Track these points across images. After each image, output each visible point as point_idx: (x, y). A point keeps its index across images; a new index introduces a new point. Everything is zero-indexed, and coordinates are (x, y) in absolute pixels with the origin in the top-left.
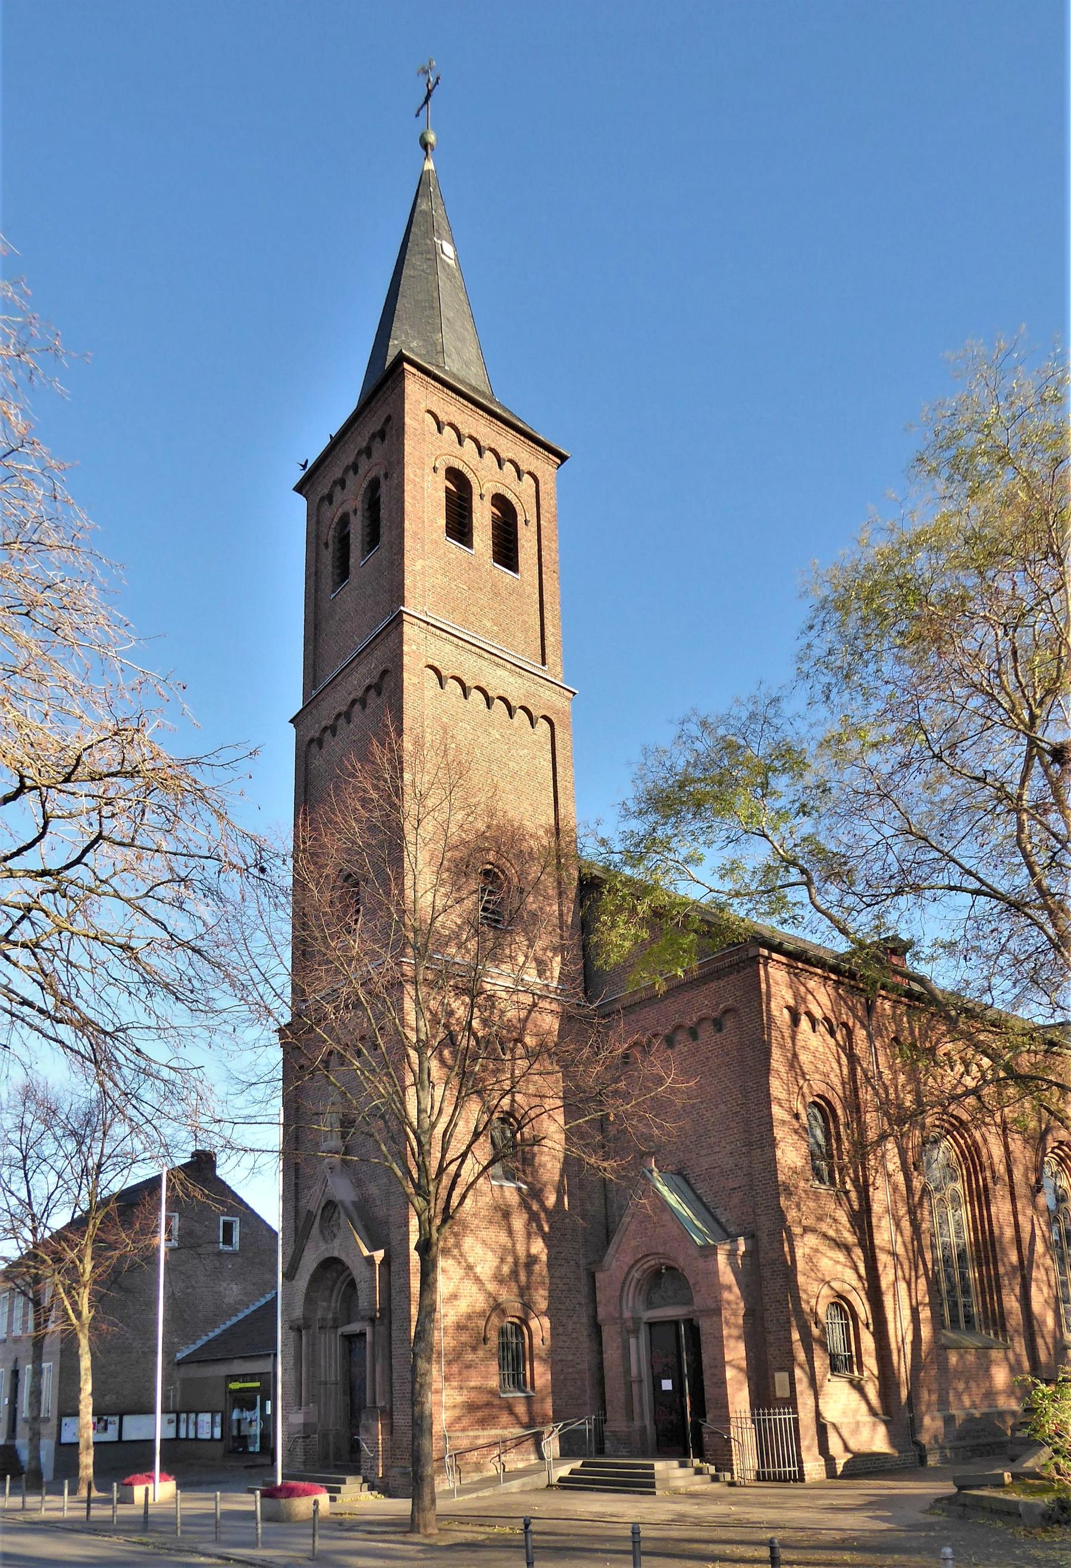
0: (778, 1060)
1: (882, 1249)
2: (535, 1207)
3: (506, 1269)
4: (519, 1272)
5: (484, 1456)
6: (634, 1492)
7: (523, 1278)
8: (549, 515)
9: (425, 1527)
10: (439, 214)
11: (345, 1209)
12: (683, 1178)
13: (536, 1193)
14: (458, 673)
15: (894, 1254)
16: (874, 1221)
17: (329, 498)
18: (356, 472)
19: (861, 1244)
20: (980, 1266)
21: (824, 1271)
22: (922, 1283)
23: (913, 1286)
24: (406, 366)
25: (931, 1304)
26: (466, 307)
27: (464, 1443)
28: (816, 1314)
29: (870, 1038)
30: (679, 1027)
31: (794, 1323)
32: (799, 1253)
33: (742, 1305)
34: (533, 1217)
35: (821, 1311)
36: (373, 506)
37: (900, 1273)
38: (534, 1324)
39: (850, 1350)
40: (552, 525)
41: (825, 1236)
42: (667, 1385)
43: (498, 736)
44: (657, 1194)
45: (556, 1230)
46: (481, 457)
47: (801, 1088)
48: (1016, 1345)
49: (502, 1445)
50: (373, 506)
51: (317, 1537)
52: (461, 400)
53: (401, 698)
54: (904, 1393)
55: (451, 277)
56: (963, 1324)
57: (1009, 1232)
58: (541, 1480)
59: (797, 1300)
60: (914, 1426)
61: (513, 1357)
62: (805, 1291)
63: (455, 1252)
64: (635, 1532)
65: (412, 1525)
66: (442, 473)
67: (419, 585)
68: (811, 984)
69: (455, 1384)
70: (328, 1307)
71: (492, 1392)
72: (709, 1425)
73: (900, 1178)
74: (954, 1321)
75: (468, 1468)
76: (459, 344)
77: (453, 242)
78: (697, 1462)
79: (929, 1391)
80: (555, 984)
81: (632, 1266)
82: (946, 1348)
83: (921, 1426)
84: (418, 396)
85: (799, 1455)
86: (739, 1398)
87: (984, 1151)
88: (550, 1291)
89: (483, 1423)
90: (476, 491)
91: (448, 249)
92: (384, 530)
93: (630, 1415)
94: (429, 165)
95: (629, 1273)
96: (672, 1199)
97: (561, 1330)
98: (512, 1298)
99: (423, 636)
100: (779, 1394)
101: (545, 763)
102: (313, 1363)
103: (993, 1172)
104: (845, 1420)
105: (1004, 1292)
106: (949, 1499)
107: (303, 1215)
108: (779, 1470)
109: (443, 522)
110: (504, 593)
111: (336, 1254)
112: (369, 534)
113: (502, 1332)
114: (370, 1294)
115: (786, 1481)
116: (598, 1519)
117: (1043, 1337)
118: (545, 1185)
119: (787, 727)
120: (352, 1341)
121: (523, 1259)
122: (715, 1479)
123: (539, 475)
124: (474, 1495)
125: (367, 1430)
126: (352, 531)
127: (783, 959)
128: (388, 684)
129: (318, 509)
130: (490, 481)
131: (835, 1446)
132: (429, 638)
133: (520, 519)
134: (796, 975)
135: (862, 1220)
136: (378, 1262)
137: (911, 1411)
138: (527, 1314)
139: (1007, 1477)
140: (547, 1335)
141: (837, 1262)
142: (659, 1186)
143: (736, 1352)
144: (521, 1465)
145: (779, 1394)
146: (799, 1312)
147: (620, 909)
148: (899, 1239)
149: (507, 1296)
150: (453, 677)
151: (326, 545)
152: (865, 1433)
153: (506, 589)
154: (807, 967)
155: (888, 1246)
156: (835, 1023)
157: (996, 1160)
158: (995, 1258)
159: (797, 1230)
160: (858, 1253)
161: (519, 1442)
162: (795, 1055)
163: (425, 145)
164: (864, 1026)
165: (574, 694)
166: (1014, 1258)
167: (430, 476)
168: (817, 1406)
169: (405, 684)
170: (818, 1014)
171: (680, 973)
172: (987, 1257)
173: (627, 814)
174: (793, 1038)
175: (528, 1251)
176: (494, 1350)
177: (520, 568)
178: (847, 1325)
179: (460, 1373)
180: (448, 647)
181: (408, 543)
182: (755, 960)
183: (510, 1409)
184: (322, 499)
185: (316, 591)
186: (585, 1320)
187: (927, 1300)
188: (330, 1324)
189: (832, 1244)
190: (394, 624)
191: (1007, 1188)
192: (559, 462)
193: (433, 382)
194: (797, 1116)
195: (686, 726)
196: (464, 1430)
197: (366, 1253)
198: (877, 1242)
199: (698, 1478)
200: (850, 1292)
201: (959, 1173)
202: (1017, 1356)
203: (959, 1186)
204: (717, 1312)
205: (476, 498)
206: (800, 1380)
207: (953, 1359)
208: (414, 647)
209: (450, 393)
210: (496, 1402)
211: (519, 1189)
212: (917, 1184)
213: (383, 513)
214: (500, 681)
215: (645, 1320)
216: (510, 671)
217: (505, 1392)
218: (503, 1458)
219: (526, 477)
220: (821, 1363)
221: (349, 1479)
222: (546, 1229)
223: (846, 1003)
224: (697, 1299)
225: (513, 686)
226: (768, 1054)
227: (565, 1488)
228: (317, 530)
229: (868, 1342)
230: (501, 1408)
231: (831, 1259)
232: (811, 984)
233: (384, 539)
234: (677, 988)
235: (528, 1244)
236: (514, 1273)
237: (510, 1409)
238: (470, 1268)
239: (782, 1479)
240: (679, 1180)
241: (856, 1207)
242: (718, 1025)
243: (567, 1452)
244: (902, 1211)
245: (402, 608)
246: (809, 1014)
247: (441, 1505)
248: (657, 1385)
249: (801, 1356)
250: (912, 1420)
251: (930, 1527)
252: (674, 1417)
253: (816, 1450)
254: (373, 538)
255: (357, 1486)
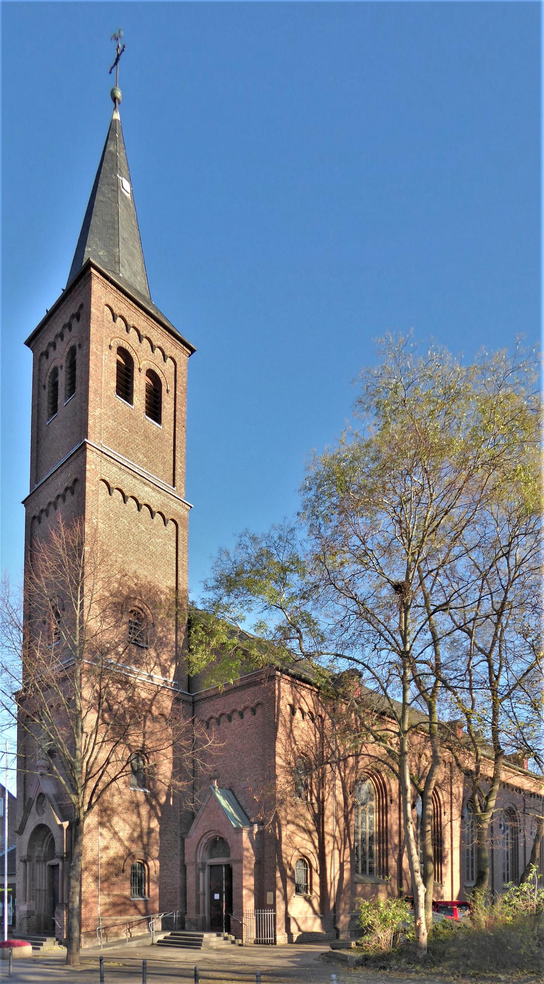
0: (281, 733)
1: (328, 834)
2: (154, 803)
3: (136, 834)
4: (142, 837)
5: (120, 929)
6: (191, 948)
7: (145, 840)
8: (182, 388)
9: (73, 962)
10: (121, 155)
11: (49, 798)
12: (231, 792)
13: (155, 795)
14: (120, 486)
15: (334, 837)
16: (325, 819)
17: (46, 354)
18: (62, 340)
19: (318, 830)
20: (379, 843)
21: (296, 843)
22: (347, 852)
23: (342, 852)
24: (93, 270)
25: (351, 862)
26: (136, 231)
27: (109, 922)
28: (290, 865)
29: (333, 725)
30: (234, 711)
31: (278, 868)
32: (284, 834)
33: (254, 858)
34: (152, 807)
35: (293, 863)
36: (72, 366)
37: (336, 846)
38: (151, 863)
39: (307, 882)
40: (183, 395)
41: (298, 825)
42: (217, 896)
43: (144, 529)
44: (217, 800)
45: (166, 815)
46: (140, 342)
47: (293, 749)
48: (392, 883)
49: (130, 925)
50: (72, 366)
51: (11, 966)
52: (129, 300)
53: (84, 499)
54: (332, 904)
55: (127, 206)
56: (368, 872)
57: (395, 828)
58: (148, 942)
59: (281, 857)
60: (335, 920)
61: (139, 880)
62: (285, 853)
63: (108, 824)
64: (144, 963)
65: (67, 961)
66: (115, 350)
67: (97, 425)
68: (304, 693)
69: (105, 893)
70: (40, 850)
71: (126, 897)
72: (233, 917)
73: (341, 798)
74: (364, 870)
75: (111, 935)
76: (130, 258)
77: (130, 180)
78: (226, 934)
79: (345, 904)
80: (171, 680)
81: (203, 836)
82: (356, 883)
83: (339, 919)
84: (100, 293)
85: (275, 932)
86: (249, 904)
87: (388, 787)
88: (160, 847)
89: (120, 913)
90: (136, 366)
91: (126, 185)
92: (78, 384)
93: (198, 911)
94: (117, 116)
95: (201, 840)
96: (224, 803)
97: (165, 867)
98: (139, 850)
99: (99, 460)
100: (268, 903)
101: (172, 549)
102: (33, 879)
103: (391, 797)
104: (301, 916)
105: (390, 857)
106: (326, 954)
107: (27, 800)
108: (265, 940)
109: (114, 384)
110: (152, 437)
111: (44, 822)
112: (69, 384)
113: (133, 867)
114: (62, 846)
115: (267, 944)
116: (166, 960)
117: (406, 880)
118: (160, 791)
119: (298, 546)
120: (54, 868)
121: (145, 830)
122: (233, 942)
123: (177, 360)
124: (112, 948)
125: (59, 914)
126: (59, 381)
127: (289, 678)
128: (78, 488)
129: (40, 360)
130: (145, 360)
131: (293, 928)
132: (103, 461)
133: (164, 389)
134: (295, 687)
135: (319, 819)
136: (65, 828)
137: (335, 913)
138: (147, 858)
139: (353, 944)
140: (158, 869)
141: (304, 839)
142: (218, 795)
143: (249, 881)
144: (140, 934)
145: (268, 903)
146: (281, 863)
147: (201, 642)
148: (337, 829)
149: (136, 849)
150: (117, 489)
151: (44, 387)
152: (310, 923)
153: (153, 434)
154: (302, 683)
155: (331, 832)
156: (315, 715)
157: (393, 791)
158: (387, 840)
159: (283, 822)
160: (315, 835)
161: (139, 923)
162: (291, 731)
163: (114, 99)
164: (331, 718)
165: (191, 507)
166: (396, 841)
167: (107, 352)
168: (286, 909)
169: (87, 490)
170: (306, 710)
171: (232, 682)
172: (383, 839)
173: (207, 588)
174: (291, 722)
175: (149, 825)
176: (128, 876)
177: (163, 422)
178: (307, 870)
179: (109, 887)
180: (115, 469)
181: (91, 396)
182: (272, 678)
183: (135, 906)
184: (42, 354)
185: (38, 418)
186: (179, 863)
187: (349, 859)
188: (42, 859)
189: (302, 830)
190: (82, 449)
191: (397, 806)
192: (190, 352)
193: (110, 285)
194: (289, 763)
195: (244, 538)
196: (110, 916)
197: (59, 822)
198: (326, 830)
199: (224, 942)
200: (309, 854)
201: (375, 797)
202: (392, 889)
203: (374, 804)
204: (241, 861)
205: (136, 371)
206: (279, 896)
207: (359, 889)
208: (93, 467)
209: (121, 294)
210: (128, 902)
211: (145, 792)
212: (350, 801)
213: (78, 373)
214: (146, 494)
215: (208, 864)
216: (153, 489)
217: (133, 897)
218: (131, 930)
219: (169, 360)
220: (290, 888)
221: (48, 939)
222: (160, 815)
223: (322, 705)
224: (232, 854)
225: (154, 499)
226: (276, 729)
227: (160, 945)
228: (39, 375)
229: (316, 879)
230: (131, 906)
231: (301, 837)
232: (304, 693)
233: (78, 389)
234: (231, 690)
235: (149, 823)
236: (140, 837)
237: (135, 906)
238: (116, 833)
239: (265, 943)
240: (229, 793)
241: (317, 812)
242: (254, 711)
243: (164, 929)
244: (341, 814)
245: (86, 440)
246: (301, 709)
247: (82, 953)
248: (212, 896)
249: (280, 884)
250: (335, 917)
251: (316, 966)
252: (219, 913)
253: (284, 930)
254: (72, 389)
255: (52, 943)
